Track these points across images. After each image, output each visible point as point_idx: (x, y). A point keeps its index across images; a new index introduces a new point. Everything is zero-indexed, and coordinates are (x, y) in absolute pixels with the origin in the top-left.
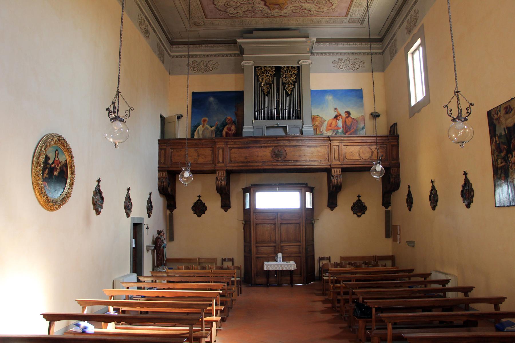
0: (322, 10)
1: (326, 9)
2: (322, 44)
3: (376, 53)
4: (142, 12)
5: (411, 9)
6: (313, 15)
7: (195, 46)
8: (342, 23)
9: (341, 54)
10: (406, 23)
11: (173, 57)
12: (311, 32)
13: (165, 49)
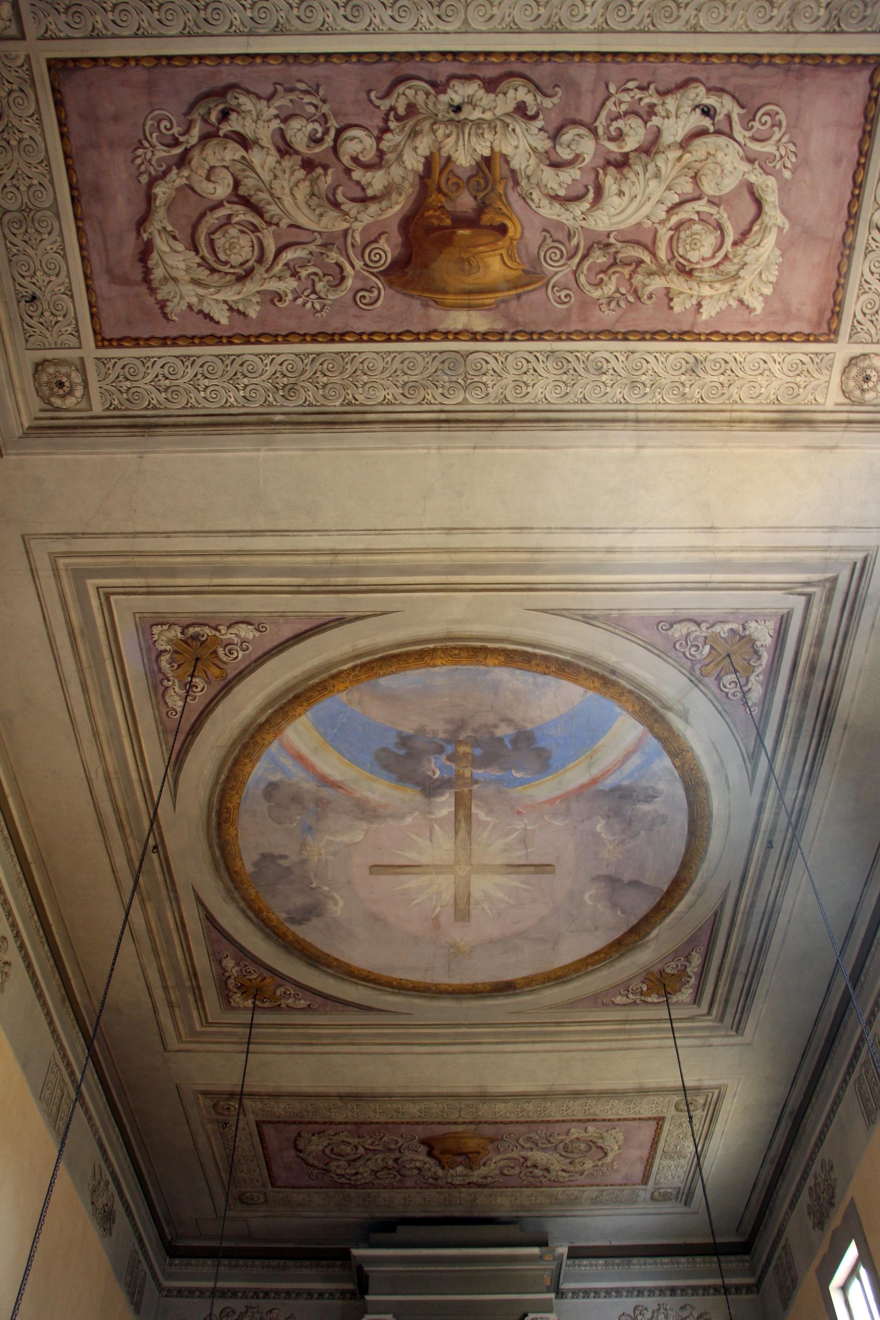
0: (579, 1168)
1: (589, 1164)
2: (585, 1262)
3: (738, 1289)
4: (107, 1159)
5: (812, 1159)
6: (556, 1183)
7: (234, 1261)
8: (633, 1201)
9: (640, 1292)
10: (805, 1199)
11: (169, 1293)
12: (553, 1227)
13: (151, 1267)
